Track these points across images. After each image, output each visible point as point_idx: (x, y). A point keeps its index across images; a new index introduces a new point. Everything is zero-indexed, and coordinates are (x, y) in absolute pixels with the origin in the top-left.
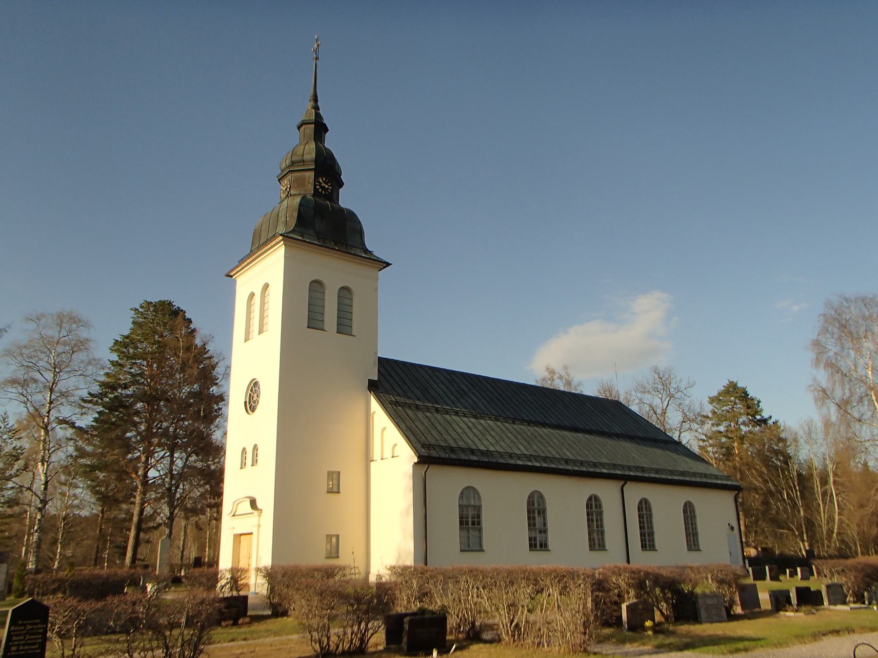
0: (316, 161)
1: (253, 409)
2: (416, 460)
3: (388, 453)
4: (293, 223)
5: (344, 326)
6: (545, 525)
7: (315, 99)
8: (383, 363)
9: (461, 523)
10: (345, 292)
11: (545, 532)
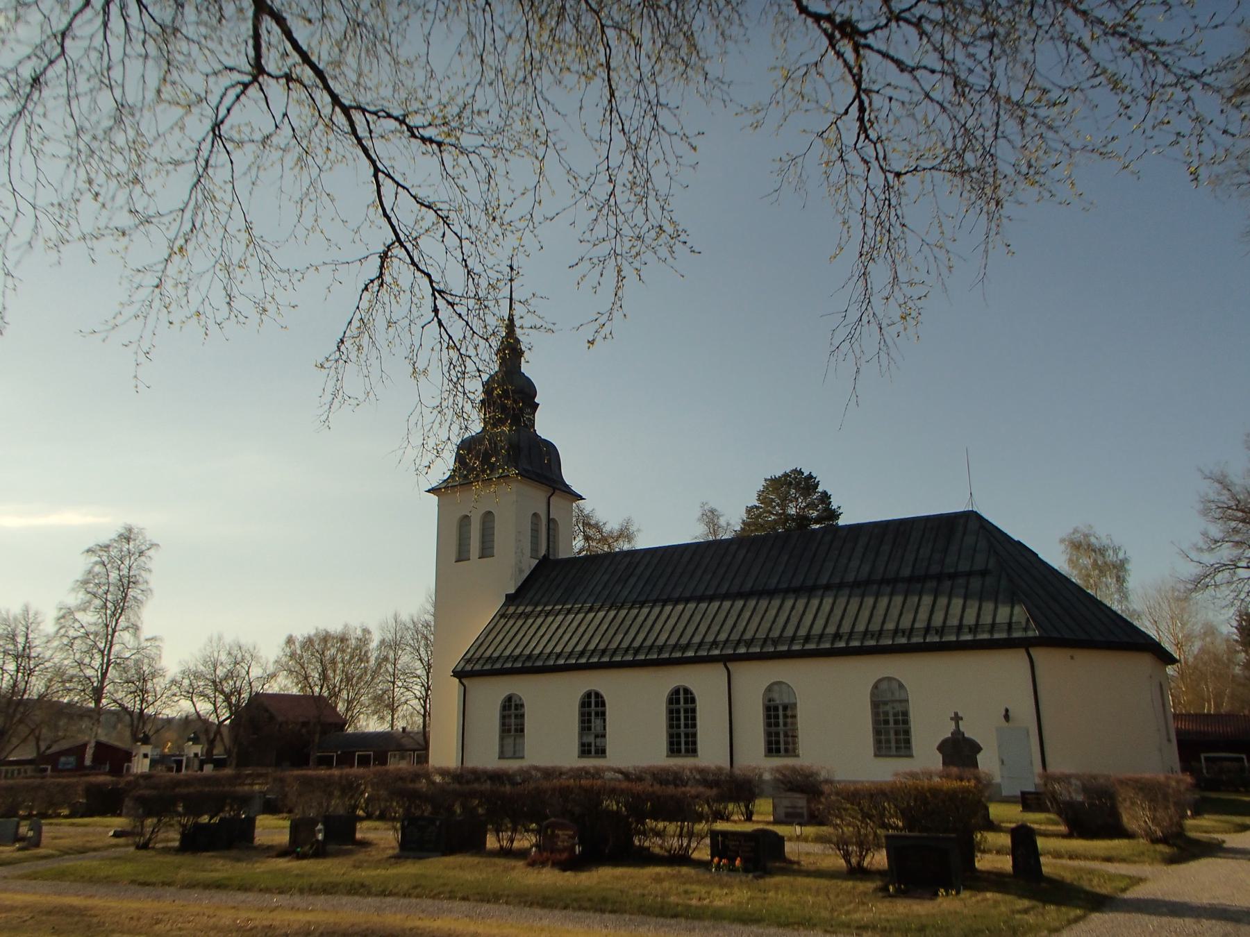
11: (604, 736)
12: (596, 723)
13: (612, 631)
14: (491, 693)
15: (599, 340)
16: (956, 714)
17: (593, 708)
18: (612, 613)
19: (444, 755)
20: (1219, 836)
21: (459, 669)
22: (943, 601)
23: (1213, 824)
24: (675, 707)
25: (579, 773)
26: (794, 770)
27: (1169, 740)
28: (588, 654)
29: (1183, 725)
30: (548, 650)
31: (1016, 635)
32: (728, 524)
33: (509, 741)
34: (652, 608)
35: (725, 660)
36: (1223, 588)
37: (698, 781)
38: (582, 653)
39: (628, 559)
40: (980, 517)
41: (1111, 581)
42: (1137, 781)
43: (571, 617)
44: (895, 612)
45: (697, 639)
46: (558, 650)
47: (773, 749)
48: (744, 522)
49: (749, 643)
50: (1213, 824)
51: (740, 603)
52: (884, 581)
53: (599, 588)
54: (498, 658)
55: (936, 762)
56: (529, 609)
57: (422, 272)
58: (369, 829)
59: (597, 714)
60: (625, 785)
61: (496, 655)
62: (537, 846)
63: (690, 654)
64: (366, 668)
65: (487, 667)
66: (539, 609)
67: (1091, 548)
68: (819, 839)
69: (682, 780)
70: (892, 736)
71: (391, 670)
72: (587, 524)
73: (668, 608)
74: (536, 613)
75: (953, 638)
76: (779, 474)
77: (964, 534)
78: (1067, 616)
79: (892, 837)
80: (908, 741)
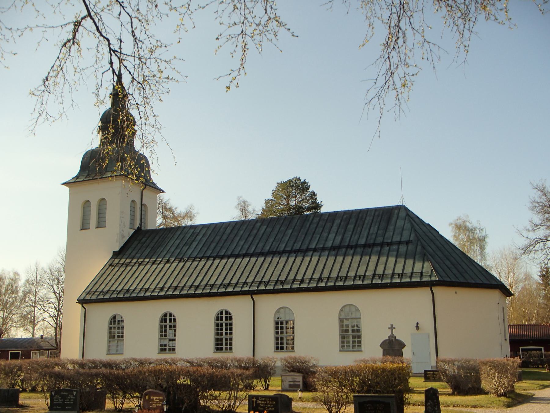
12: (170, 332)
13: (180, 276)
14: (102, 314)
15: (233, 87)
16: (392, 325)
17: (168, 322)
18: (182, 264)
19: (71, 351)
20: (532, 392)
21: (82, 298)
22: (383, 259)
23: (528, 385)
25: (159, 362)
26: (295, 359)
27: (506, 340)
28: (165, 289)
29: (516, 332)
30: (140, 287)
31: (424, 279)
32: (254, 211)
33: (114, 343)
34: (207, 261)
35: (251, 293)
36: (539, 252)
37: (236, 366)
38: (162, 289)
39: (192, 231)
40: (406, 209)
41: (477, 248)
42: (491, 362)
43: (154, 266)
44: (355, 265)
45: (234, 281)
46: (147, 286)
47: (279, 347)
48: (263, 209)
49: (266, 284)
50: (528, 385)
51: (261, 259)
52: (349, 247)
53: (173, 249)
54: (108, 291)
55: (379, 353)
56: (128, 261)
57: (104, 37)
58: (25, 398)
59: (170, 327)
60: (192, 369)
61: (106, 289)
62: (139, 406)
63: (230, 289)
64: (15, 297)
65: (101, 297)
66: (135, 261)
67: (466, 229)
68: (314, 400)
69: (226, 367)
70: (351, 340)
71: (33, 298)
72: (164, 208)
73: (217, 262)
74: (132, 264)
75: (389, 281)
76: (286, 179)
77: (397, 219)
78: (453, 268)
79: (357, 396)
80: (359, 342)
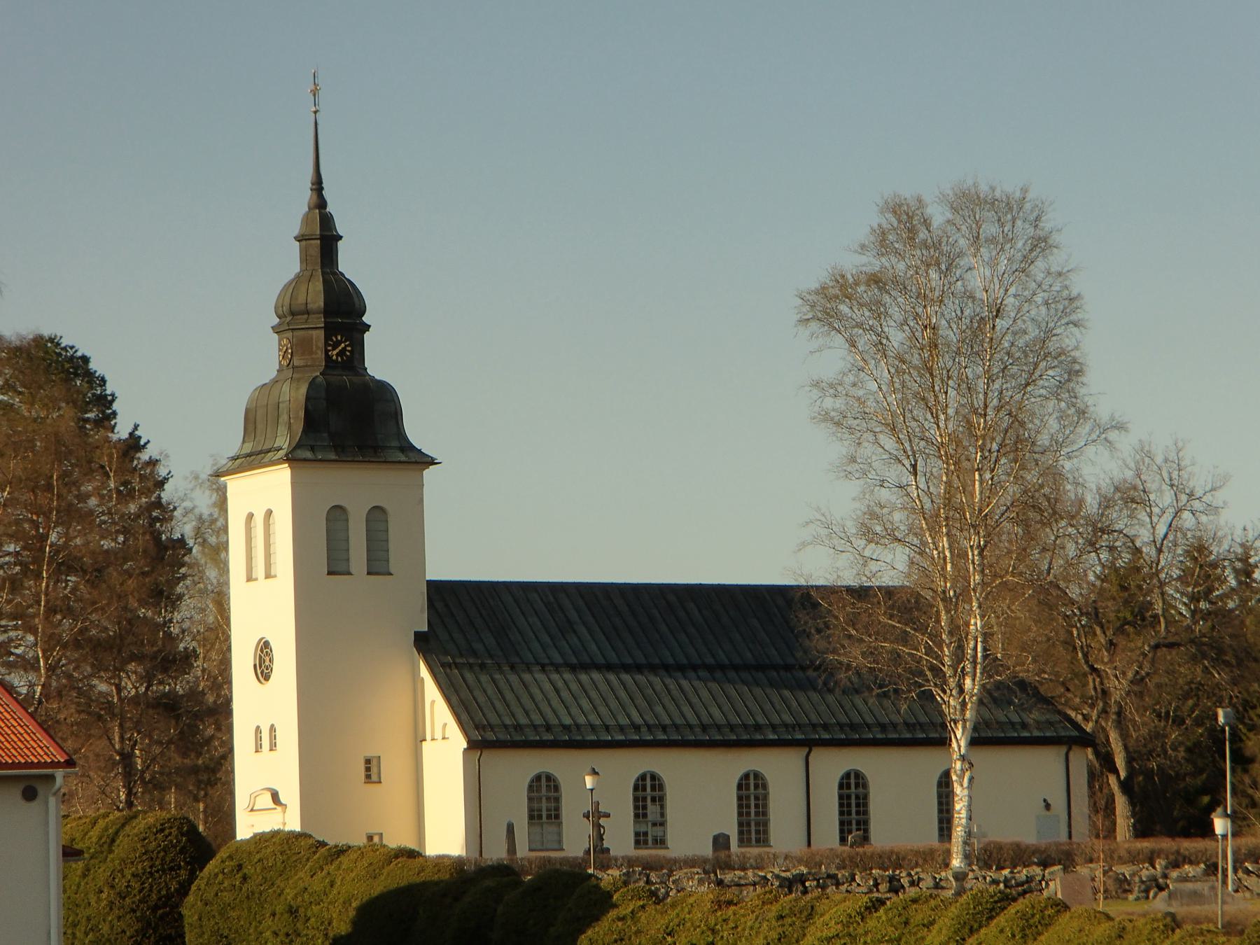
0: (328, 311)
1: (267, 678)
2: (465, 745)
3: (438, 735)
4: (299, 427)
5: (378, 565)
6: (662, 815)
7: (318, 185)
8: (444, 596)
9: (531, 817)
10: (377, 516)
11: (663, 824)
12: (652, 809)
24: (845, 791)
59: (653, 800)
